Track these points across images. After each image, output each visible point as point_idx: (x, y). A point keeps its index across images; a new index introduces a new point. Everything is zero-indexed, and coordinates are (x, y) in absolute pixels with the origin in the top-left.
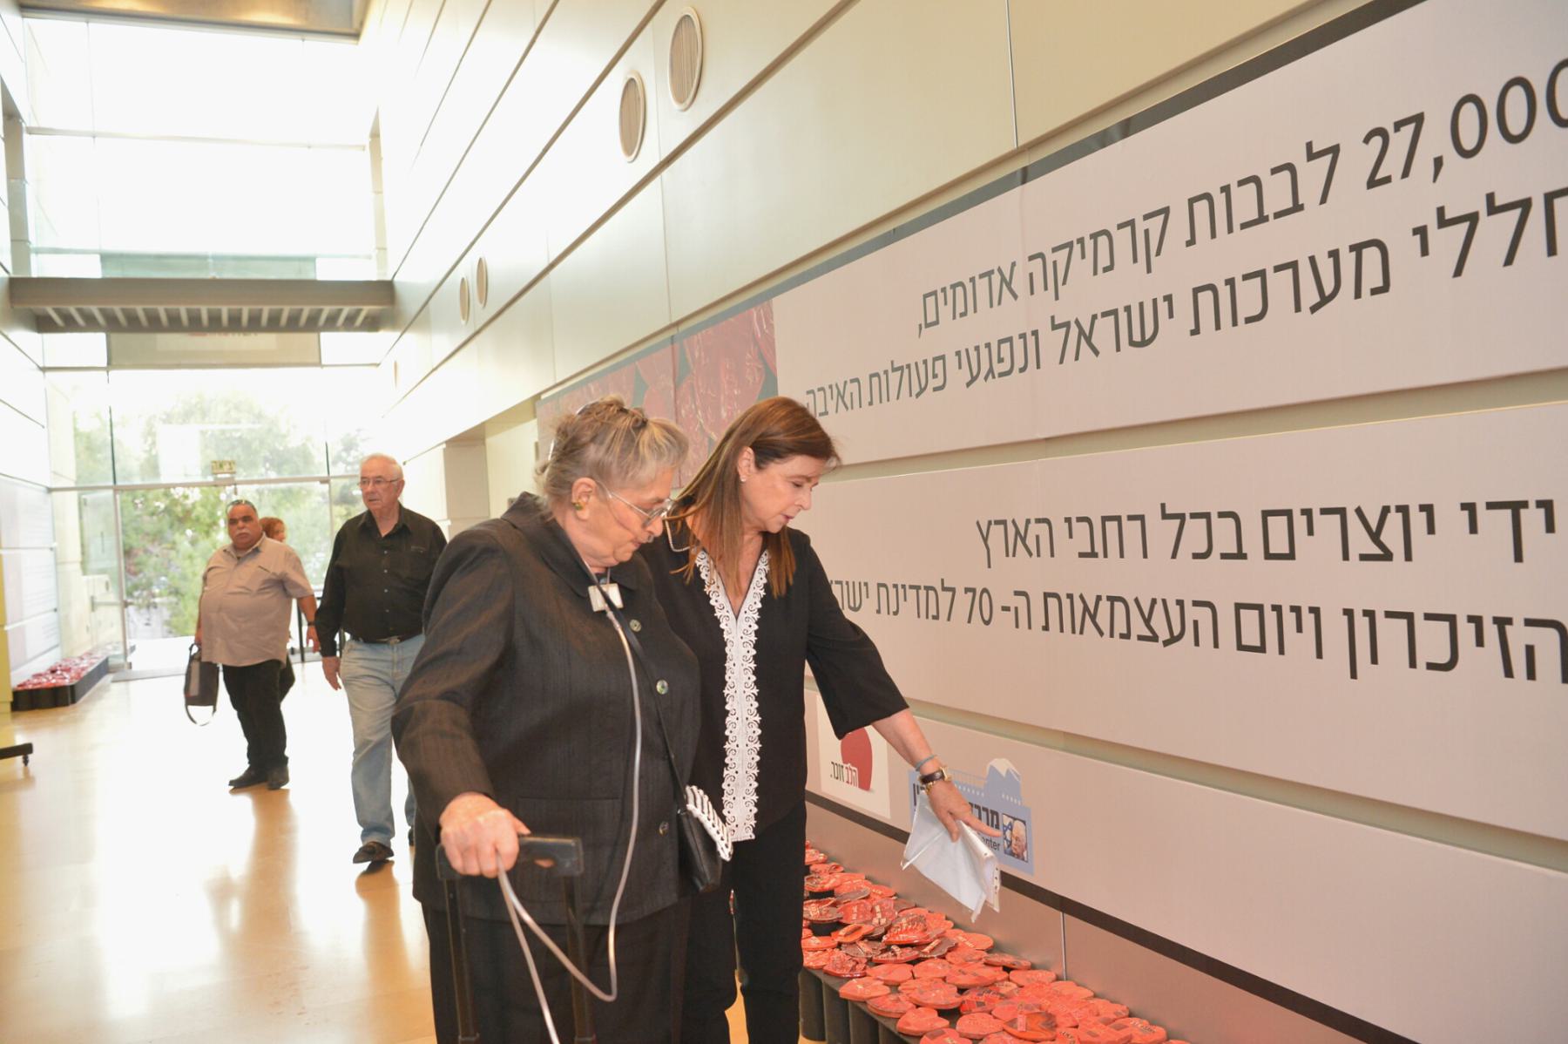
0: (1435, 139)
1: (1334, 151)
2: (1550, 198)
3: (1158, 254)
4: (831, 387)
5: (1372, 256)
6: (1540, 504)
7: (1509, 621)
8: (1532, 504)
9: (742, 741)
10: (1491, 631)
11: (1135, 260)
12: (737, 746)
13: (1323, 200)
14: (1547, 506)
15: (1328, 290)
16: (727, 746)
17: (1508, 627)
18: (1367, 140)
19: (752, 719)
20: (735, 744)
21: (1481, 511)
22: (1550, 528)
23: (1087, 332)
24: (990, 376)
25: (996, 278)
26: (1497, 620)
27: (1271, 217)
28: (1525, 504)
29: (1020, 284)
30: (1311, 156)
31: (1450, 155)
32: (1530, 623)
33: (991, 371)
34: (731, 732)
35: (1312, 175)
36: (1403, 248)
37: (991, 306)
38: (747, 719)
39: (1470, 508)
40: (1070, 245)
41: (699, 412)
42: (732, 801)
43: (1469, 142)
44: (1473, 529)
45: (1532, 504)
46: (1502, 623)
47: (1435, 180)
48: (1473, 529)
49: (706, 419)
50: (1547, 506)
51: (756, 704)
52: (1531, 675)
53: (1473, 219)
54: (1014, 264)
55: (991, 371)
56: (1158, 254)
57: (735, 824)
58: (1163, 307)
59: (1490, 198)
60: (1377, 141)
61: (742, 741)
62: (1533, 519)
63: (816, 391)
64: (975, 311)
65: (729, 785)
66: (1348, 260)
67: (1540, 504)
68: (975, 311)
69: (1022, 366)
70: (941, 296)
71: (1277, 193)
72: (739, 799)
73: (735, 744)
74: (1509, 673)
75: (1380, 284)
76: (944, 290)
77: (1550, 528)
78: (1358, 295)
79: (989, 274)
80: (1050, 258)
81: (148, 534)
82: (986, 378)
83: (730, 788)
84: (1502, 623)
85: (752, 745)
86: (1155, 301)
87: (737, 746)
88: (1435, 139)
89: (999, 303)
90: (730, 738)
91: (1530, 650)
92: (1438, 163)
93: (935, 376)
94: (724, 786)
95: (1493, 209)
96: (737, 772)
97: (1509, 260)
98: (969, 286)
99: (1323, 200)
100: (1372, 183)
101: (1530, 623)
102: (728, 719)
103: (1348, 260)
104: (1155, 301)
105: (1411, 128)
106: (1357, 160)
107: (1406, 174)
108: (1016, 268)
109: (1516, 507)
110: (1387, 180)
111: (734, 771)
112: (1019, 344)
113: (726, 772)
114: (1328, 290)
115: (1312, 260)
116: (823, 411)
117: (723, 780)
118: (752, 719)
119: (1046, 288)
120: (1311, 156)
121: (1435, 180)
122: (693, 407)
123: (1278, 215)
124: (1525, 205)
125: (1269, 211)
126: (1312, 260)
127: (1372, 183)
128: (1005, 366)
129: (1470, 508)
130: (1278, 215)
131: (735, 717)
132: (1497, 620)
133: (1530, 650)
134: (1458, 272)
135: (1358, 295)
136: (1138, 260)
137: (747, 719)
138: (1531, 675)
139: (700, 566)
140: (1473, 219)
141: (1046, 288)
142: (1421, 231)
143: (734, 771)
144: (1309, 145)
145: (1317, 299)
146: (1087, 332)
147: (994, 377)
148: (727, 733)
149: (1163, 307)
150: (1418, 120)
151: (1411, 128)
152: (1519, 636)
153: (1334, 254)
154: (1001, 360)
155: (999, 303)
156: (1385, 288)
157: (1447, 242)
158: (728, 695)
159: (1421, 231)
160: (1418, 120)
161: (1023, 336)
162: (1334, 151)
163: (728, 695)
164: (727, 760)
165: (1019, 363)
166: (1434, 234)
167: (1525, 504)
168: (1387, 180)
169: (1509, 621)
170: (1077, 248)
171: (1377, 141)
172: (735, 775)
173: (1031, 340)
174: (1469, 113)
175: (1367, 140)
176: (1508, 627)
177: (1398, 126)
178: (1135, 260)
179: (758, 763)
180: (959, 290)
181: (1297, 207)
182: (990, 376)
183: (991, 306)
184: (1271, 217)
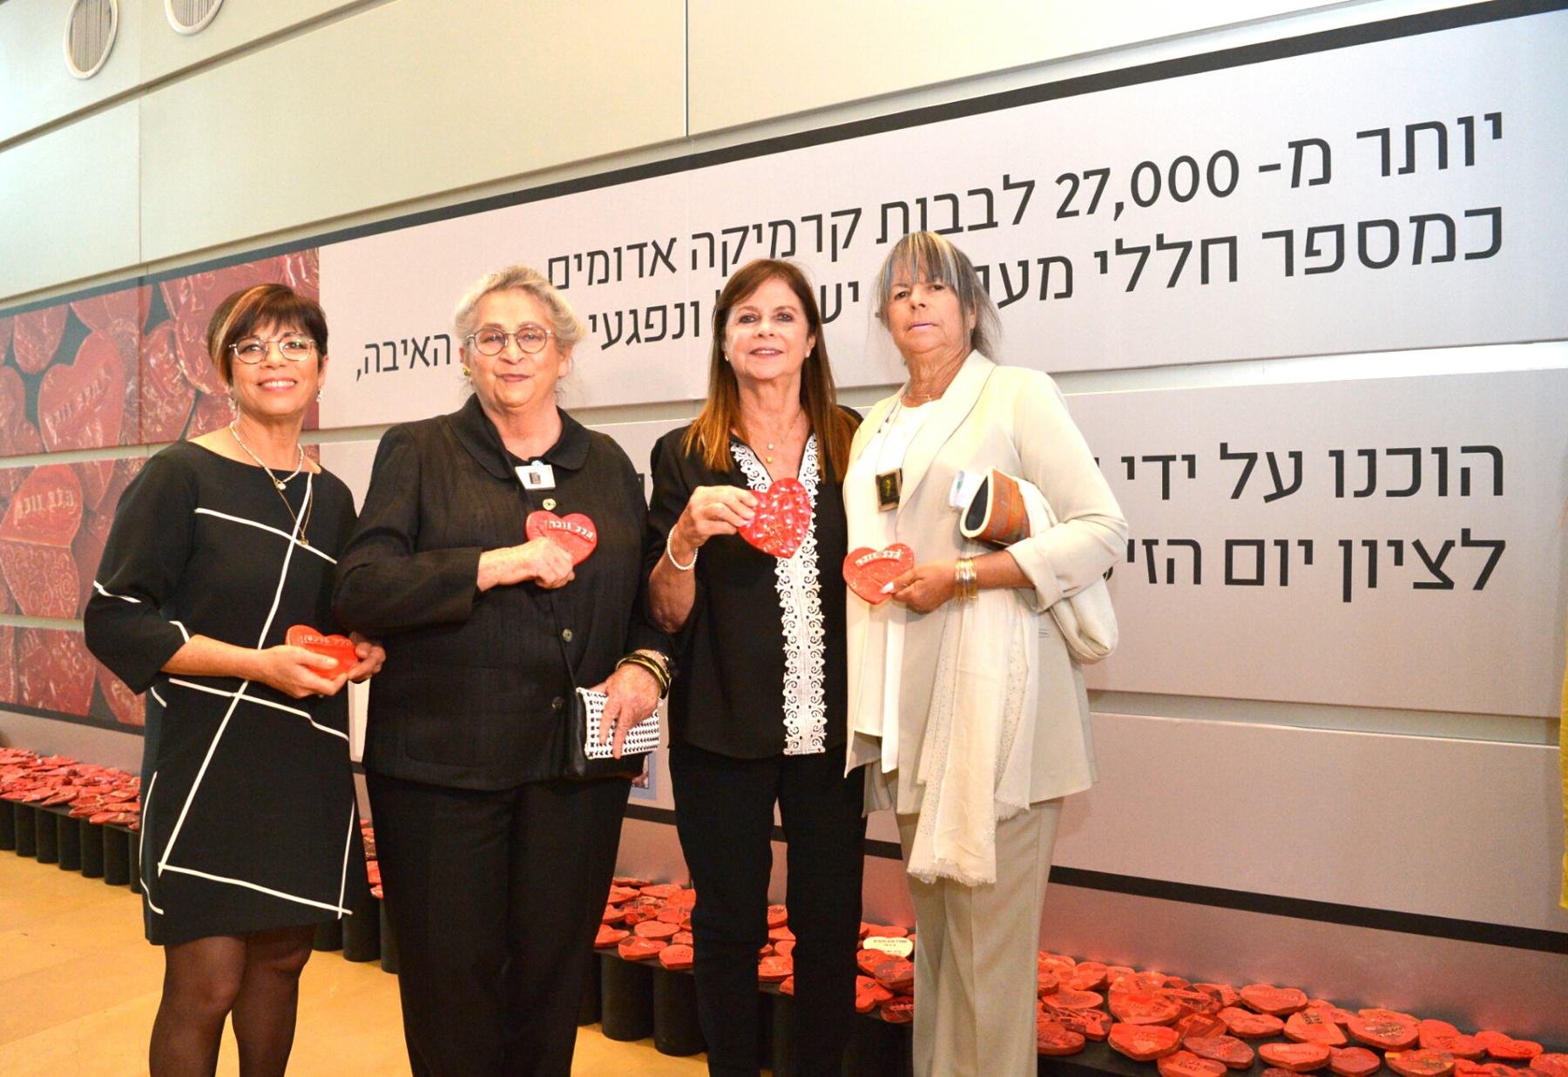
0: (1117, 188)
1: (1030, 185)
2: (1206, 244)
3: (846, 245)
4: (404, 342)
5: (1057, 270)
6: (1184, 458)
7: (1156, 542)
8: (1179, 458)
9: (803, 643)
10: (1140, 551)
11: (820, 249)
12: (798, 647)
13: (1017, 221)
14: (1190, 459)
15: (614, 336)
16: (786, 648)
17: (1154, 547)
18: (1060, 181)
19: (813, 617)
20: (795, 645)
21: (1138, 463)
22: (1192, 474)
23: (421, 349)
24: (635, 340)
25: (649, 252)
26: (1145, 542)
27: (966, 229)
28: (1173, 458)
29: (680, 257)
30: (1007, 185)
31: (1129, 202)
32: (1171, 542)
33: (636, 335)
34: (790, 632)
35: (1007, 203)
36: (1086, 268)
37: (641, 275)
38: (808, 617)
39: (1129, 461)
40: (745, 230)
41: (182, 363)
42: (795, 710)
43: (1145, 195)
44: (1131, 476)
45: (1179, 458)
46: (1150, 544)
47: (1115, 219)
48: (1131, 476)
49: (193, 370)
50: (1190, 459)
51: (818, 601)
52: (1170, 580)
53: (1145, 251)
54: (673, 240)
55: (636, 335)
56: (846, 245)
57: (798, 736)
58: (847, 293)
59: (1160, 237)
60: (1068, 184)
61: (803, 643)
62: (1178, 469)
63: (381, 346)
64: (619, 278)
65: (790, 692)
66: (1036, 272)
67: (1184, 458)
68: (619, 278)
69: (677, 331)
70: (573, 263)
71: (973, 211)
72: (804, 707)
73: (795, 645)
74: (1153, 579)
75: (1063, 290)
76: (578, 257)
77: (1192, 474)
78: (1043, 296)
79: (641, 247)
80: (827, 222)
81: (527, 288)
82: (628, 342)
83: (792, 695)
84: (1150, 544)
85: (814, 647)
86: (839, 287)
87: (798, 647)
88: (1117, 188)
89: (652, 274)
90: (789, 639)
91: (1171, 563)
92: (1119, 207)
93: (649, 326)
94: (785, 693)
95: (1161, 245)
96: (798, 677)
97: (1172, 283)
98: (613, 257)
99: (1017, 221)
100: (1062, 213)
101: (1171, 542)
102: (783, 618)
103: (1036, 272)
104: (839, 287)
105: (1097, 178)
106: (1049, 196)
107: (1092, 210)
108: (675, 244)
109: (1166, 460)
110: (1076, 213)
111: (795, 675)
112: (674, 315)
113: (786, 677)
114: (614, 336)
115: (605, 316)
116: (391, 365)
117: (783, 686)
118: (813, 617)
119: (712, 264)
120: (1007, 185)
121: (1115, 219)
122: (172, 356)
123: (971, 228)
124: (1187, 246)
125: (964, 222)
126: (605, 316)
127: (1062, 213)
128: (657, 331)
129: (1129, 461)
130: (971, 228)
131: (793, 615)
132: (1145, 542)
133: (1171, 563)
134: (1131, 288)
135: (1043, 296)
136: (676, 267)
137: (808, 617)
138: (1170, 580)
139: (740, 461)
140: (1145, 251)
141: (712, 264)
142: (1103, 256)
143: (795, 675)
144: (1006, 178)
145: (1005, 297)
146: (421, 349)
147: (639, 341)
148: (785, 633)
149: (847, 293)
150: (1105, 173)
151: (1097, 178)
152: (1162, 553)
153: (619, 314)
154: (649, 326)
155: (652, 274)
156: (1068, 293)
157: (1123, 266)
158: (781, 591)
159: (1103, 256)
160: (1105, 173)
161: (681, 306)
162: (1030, 185)
163: (781, 591)
164: (787, 664)
165: (673, 327)
166: (1112, 258)
167: (1173, 458)
168: (1076, 213)
169: (1156, 542)
170: (753, 234)
171: (1068, 184)
172: (797, 681)
173: (689, 311)
174: (1146, 176)
175: (1060, 181)
176: (1154, 547)
177: (1087, 175)
178: (820, 249)
179: (823, 667)
180: (599, 260)
181: (991, 223)
182: (635, 340)
183: (641, 275)
184: (966, 229)
